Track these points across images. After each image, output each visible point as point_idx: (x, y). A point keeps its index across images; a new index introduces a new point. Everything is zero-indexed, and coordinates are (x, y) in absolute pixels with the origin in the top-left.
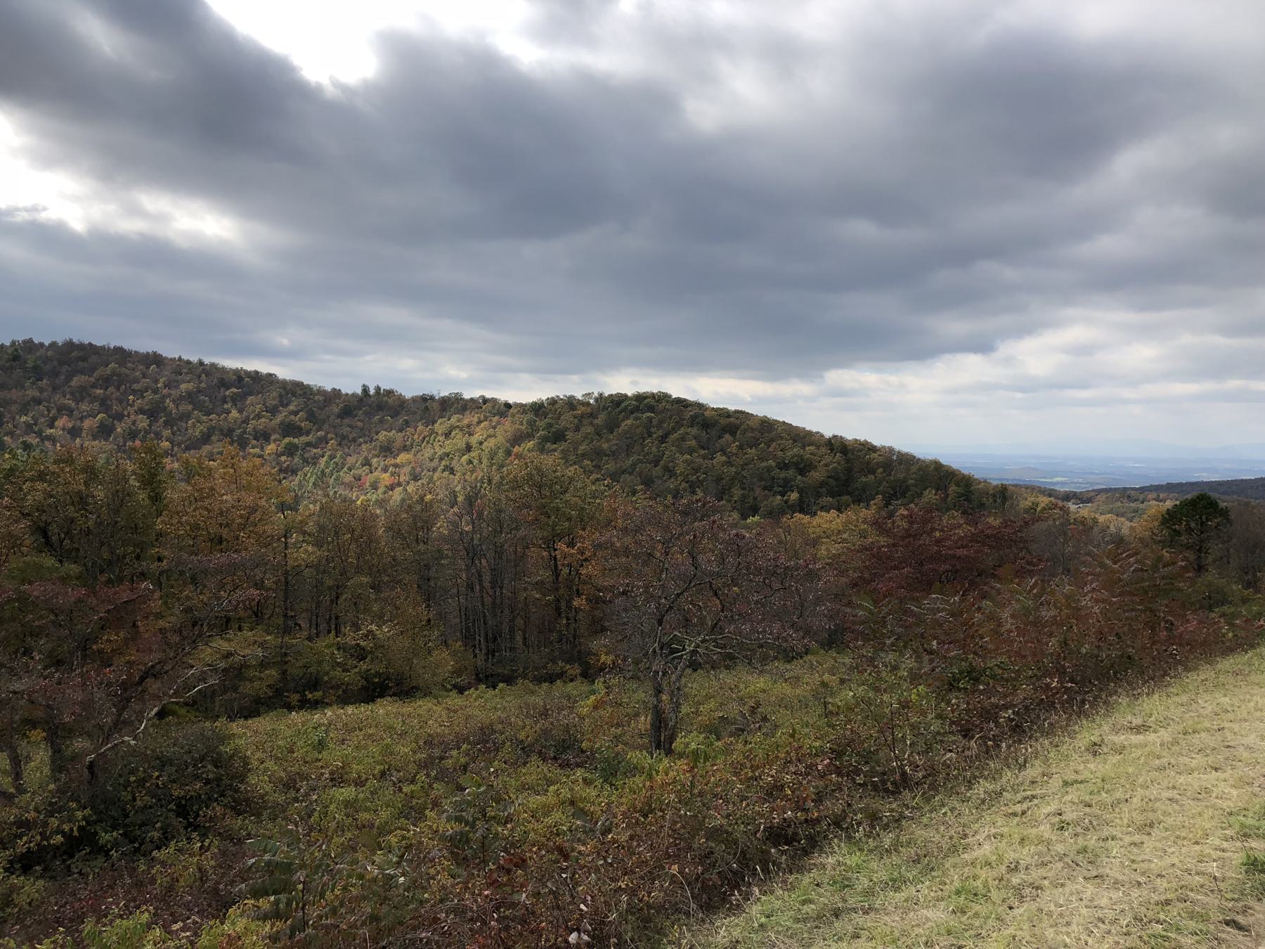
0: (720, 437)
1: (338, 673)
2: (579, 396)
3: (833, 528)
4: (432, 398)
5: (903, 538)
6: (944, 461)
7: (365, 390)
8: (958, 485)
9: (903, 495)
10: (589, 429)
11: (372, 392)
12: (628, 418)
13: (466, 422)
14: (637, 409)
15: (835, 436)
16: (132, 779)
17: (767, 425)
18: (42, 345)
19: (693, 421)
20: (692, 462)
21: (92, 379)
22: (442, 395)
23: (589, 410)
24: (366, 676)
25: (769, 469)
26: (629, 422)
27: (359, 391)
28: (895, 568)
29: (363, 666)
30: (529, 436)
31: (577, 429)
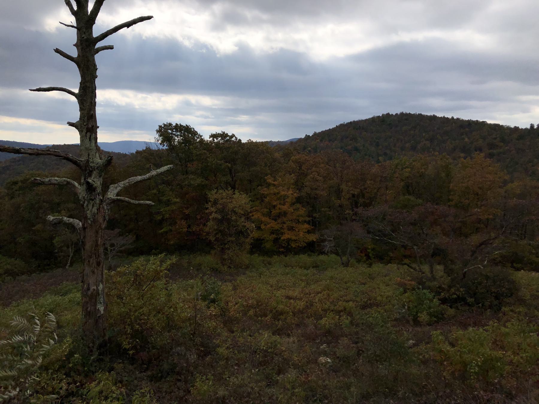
11: (163, 126)
16: (476, 281)
18: (392, 115)
27: (529, 127)
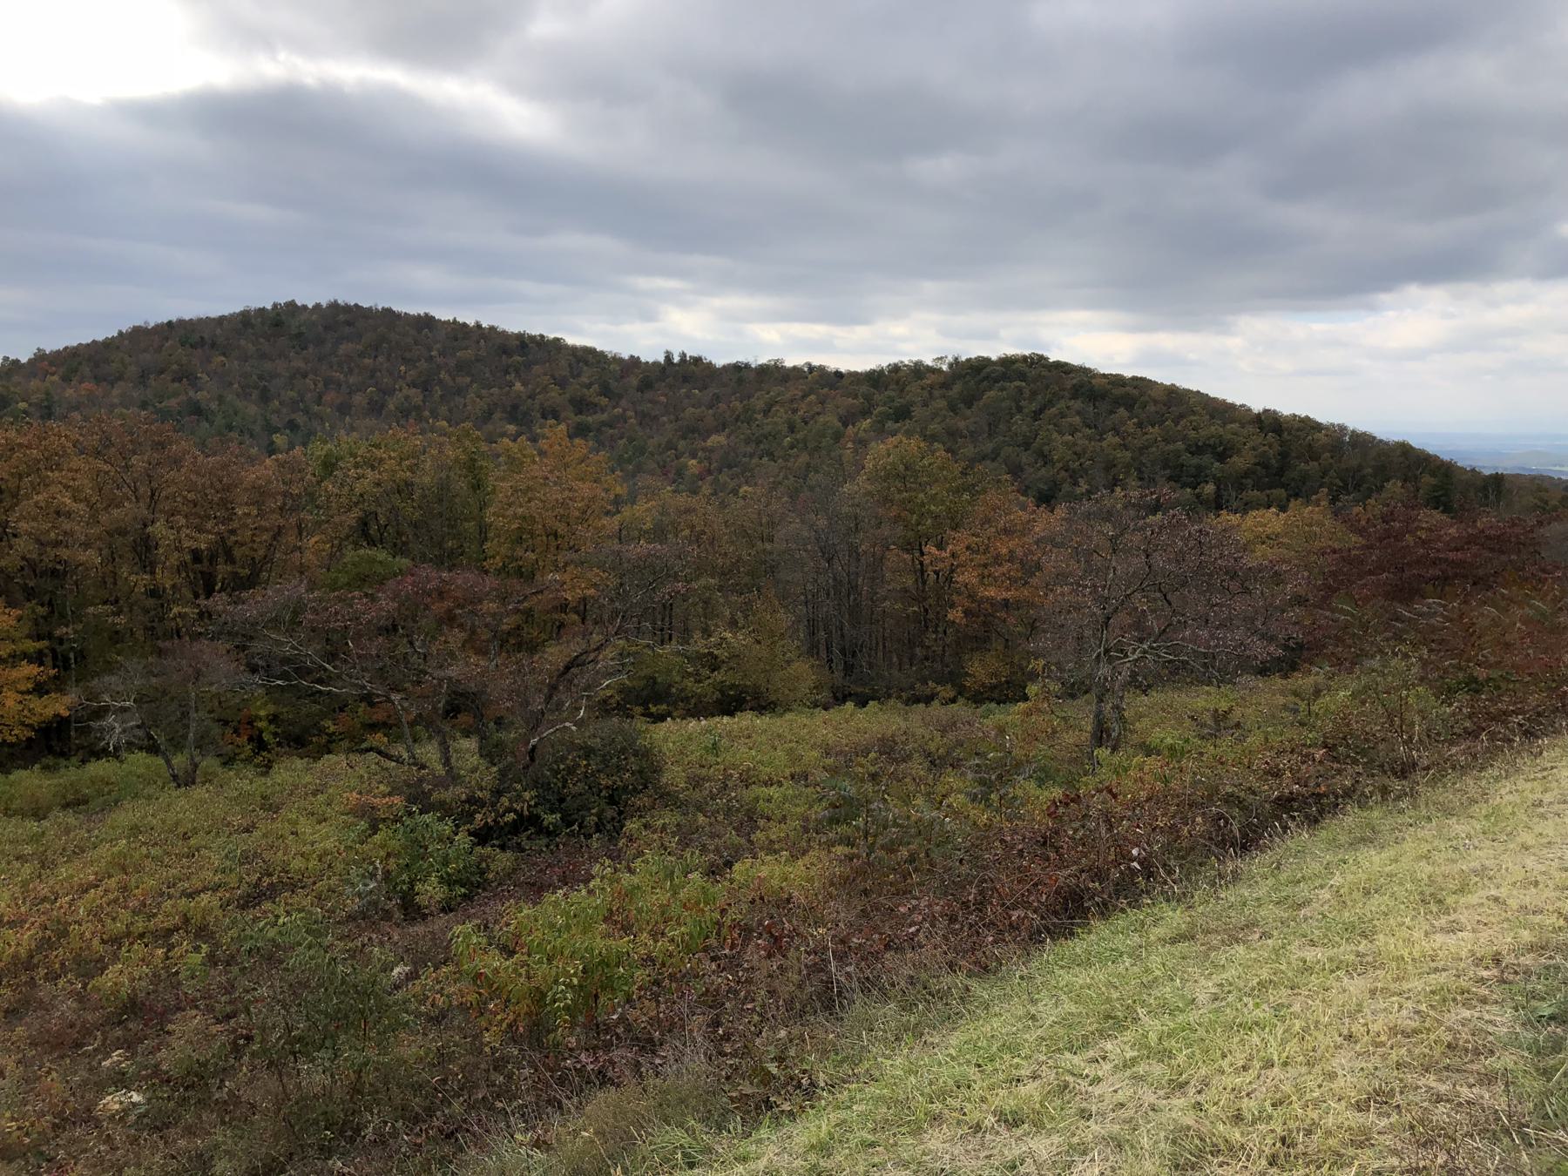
0: (1112, 412)
1: (689, 683)
2: (929, 361)
3: (1264, 530)
4: (747, 366)
5: (1381, 540)
6: (1415, 443)
7: (668, 357)
8: (1433, 475)
9: (1357, 487)
10: (942, 403)
11: (676, 359)
12: (990, 389)
13: (788, 396)
14: (1004, 377)
15: (1266, 411)
17: (1174, 395)
18: (305, 307)
19: (1076, 392)
20: (1075, 444)
21: (360, 347)
22: (760, 362)
23: (941, 379)
24: (721, 688)
25: (1178, 454)
26: (992, 393)
27: (662, 359)
28: (1371, 573)
29: (718, 676)
30: (865, 413)
31: (926, 405)
